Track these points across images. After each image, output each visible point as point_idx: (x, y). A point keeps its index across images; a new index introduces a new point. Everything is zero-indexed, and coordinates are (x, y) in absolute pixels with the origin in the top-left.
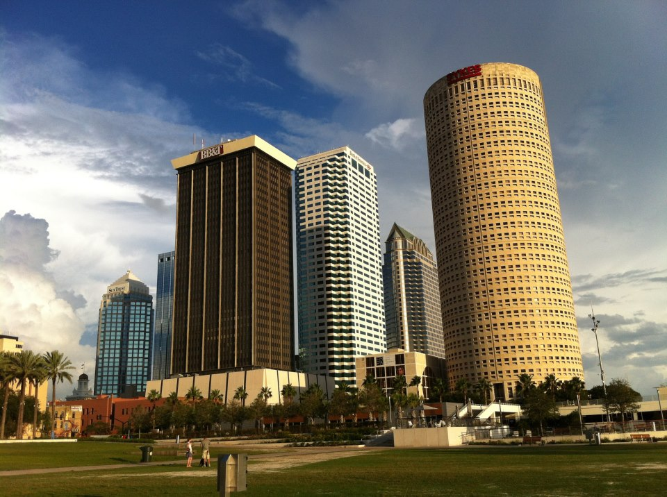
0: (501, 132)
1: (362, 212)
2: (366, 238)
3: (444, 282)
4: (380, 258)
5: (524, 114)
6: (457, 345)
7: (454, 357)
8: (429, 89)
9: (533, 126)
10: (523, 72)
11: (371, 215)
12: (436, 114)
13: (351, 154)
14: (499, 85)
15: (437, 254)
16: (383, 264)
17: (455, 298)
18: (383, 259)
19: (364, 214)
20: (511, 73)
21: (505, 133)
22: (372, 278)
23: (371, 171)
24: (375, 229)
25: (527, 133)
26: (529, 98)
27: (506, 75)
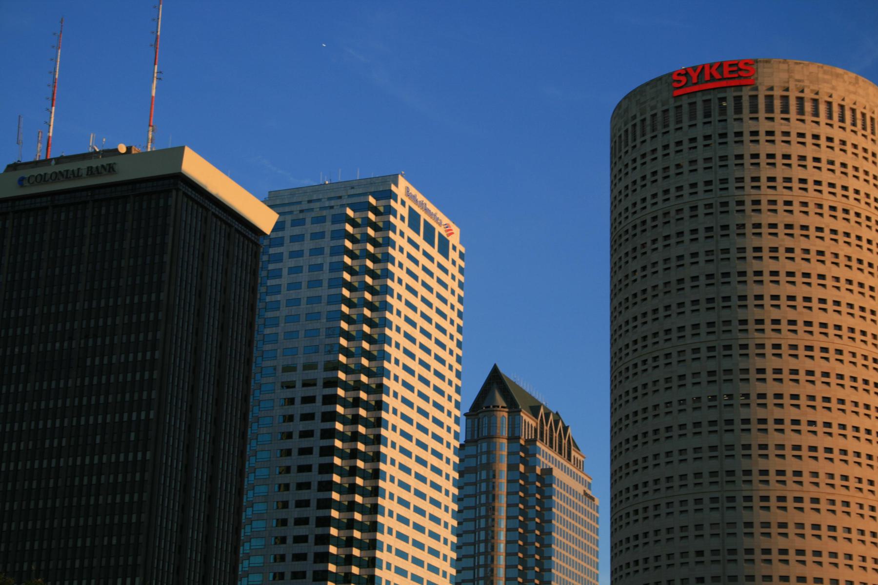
0: (789, 226)
1: (425, 269)
2: (427, 367)
3: (625, 447)
4: (457, 421)
5: (845, 188)
6: (641, 516)
7: (632, 568)
8: (628, 97)
9: (863, 219)
10: (852, 88)
11: (445, 324)
12: (639, 161)
13: (408, 194)
14: (793, 114)
15: (613, 547)
16: (462, 439)
17: (646, 535)
18: (463, 420)
19: (429, 320)
20: (825, 89)
21: (797, 231)
22: (433, 518)
23: (454, 239)
24: (452, 330)
25: (847, 235)
26: (859, 151)
27: (812, 91)
